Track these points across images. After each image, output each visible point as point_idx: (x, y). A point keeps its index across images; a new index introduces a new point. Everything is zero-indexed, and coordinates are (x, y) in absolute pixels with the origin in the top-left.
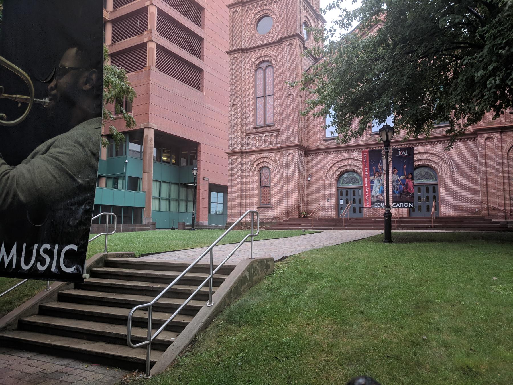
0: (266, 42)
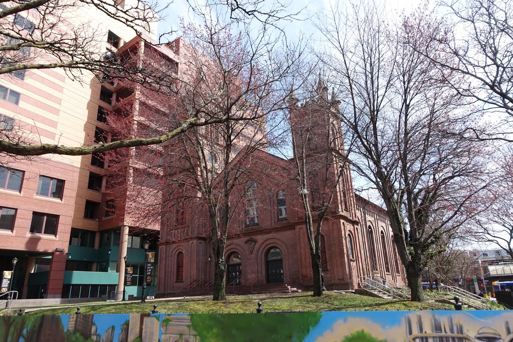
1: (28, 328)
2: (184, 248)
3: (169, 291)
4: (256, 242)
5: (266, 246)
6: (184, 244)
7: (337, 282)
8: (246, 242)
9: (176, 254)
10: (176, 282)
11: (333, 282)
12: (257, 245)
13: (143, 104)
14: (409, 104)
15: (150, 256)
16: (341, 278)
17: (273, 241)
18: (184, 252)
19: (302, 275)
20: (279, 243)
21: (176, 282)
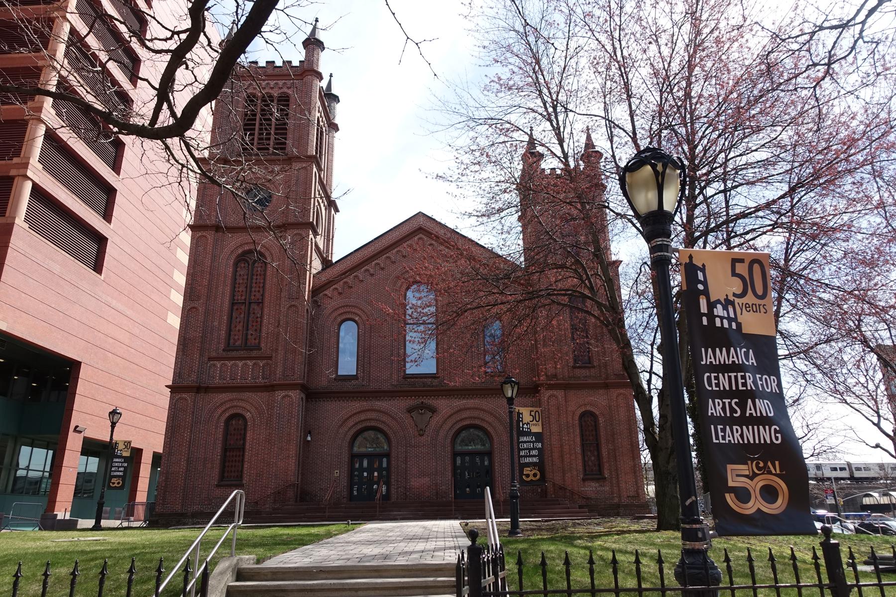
1: (117, 23)
2: (251, 406)
3: (196, 508)
4: (433, 410)
5: (457, 422)
6: (257, 398)
7: (625, 501)
8: (410, 411)
9: (223, 419)
10: (218, 486)
11: (616, 500)
12: (436, 420)
13: (51, 136)
14: (769, 225)
15: (527, 418)
16: (632, 494)
17: (476, 413)
18: (248, 415)
19: (554, 485)
20: (490, 419)
21: (218, 486)
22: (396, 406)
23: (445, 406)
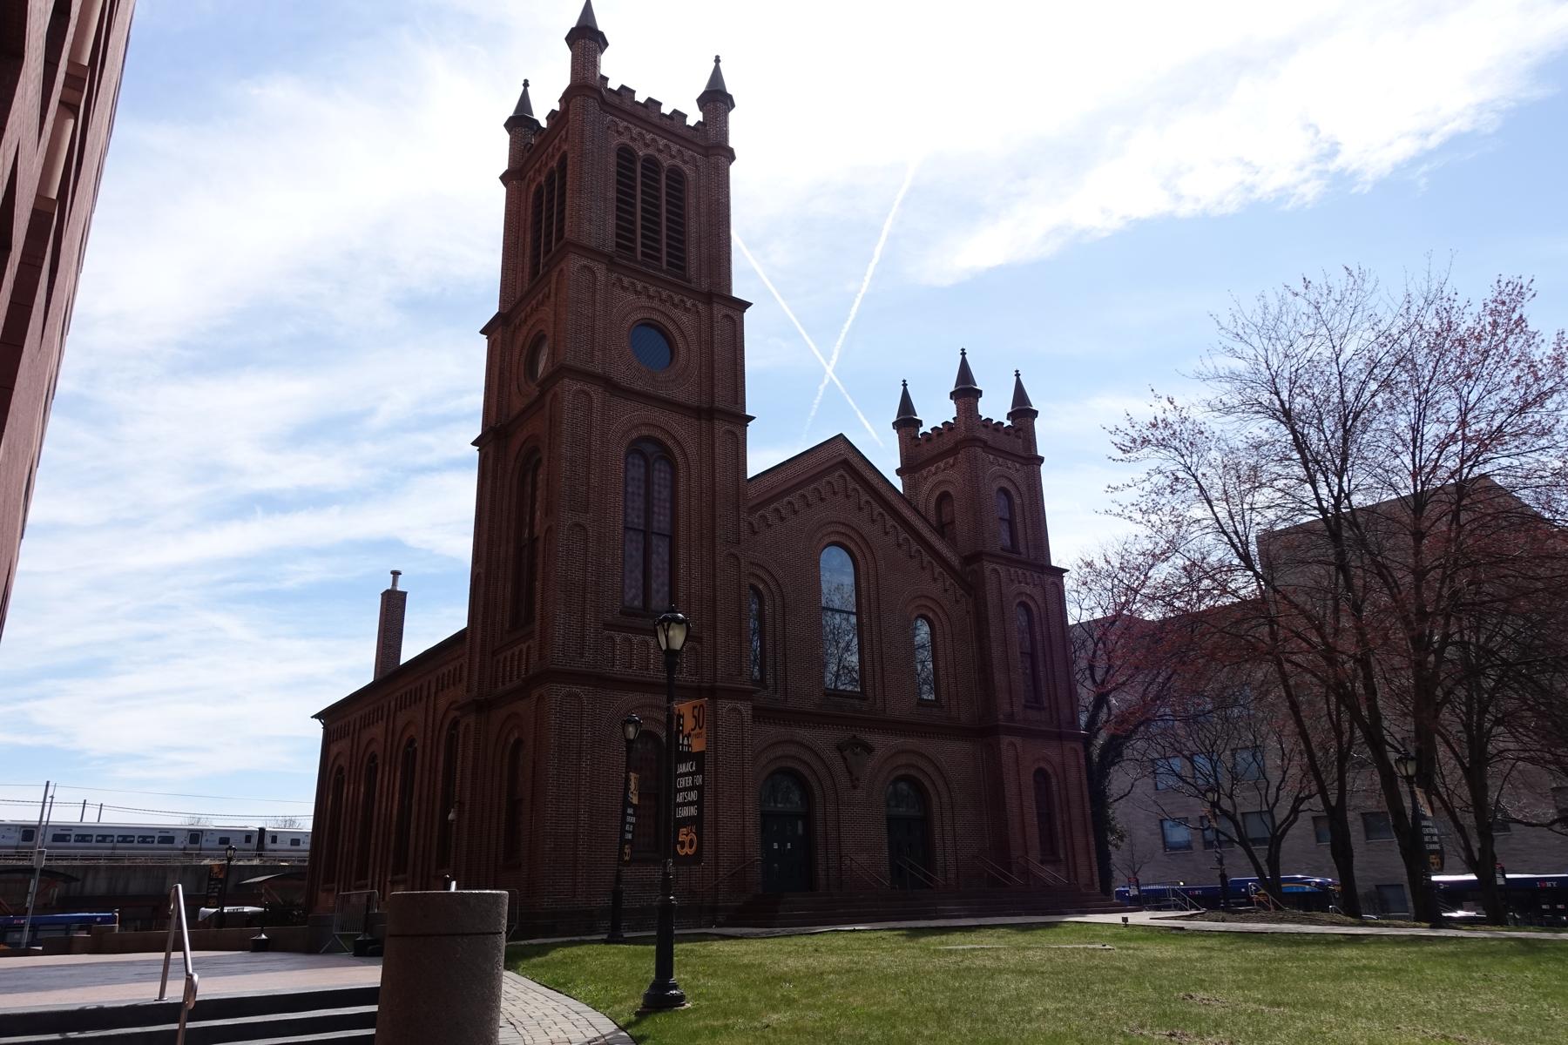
0: (663, 393)
4: (869, 749)
22: (823, 739)
23: (882, 743)
